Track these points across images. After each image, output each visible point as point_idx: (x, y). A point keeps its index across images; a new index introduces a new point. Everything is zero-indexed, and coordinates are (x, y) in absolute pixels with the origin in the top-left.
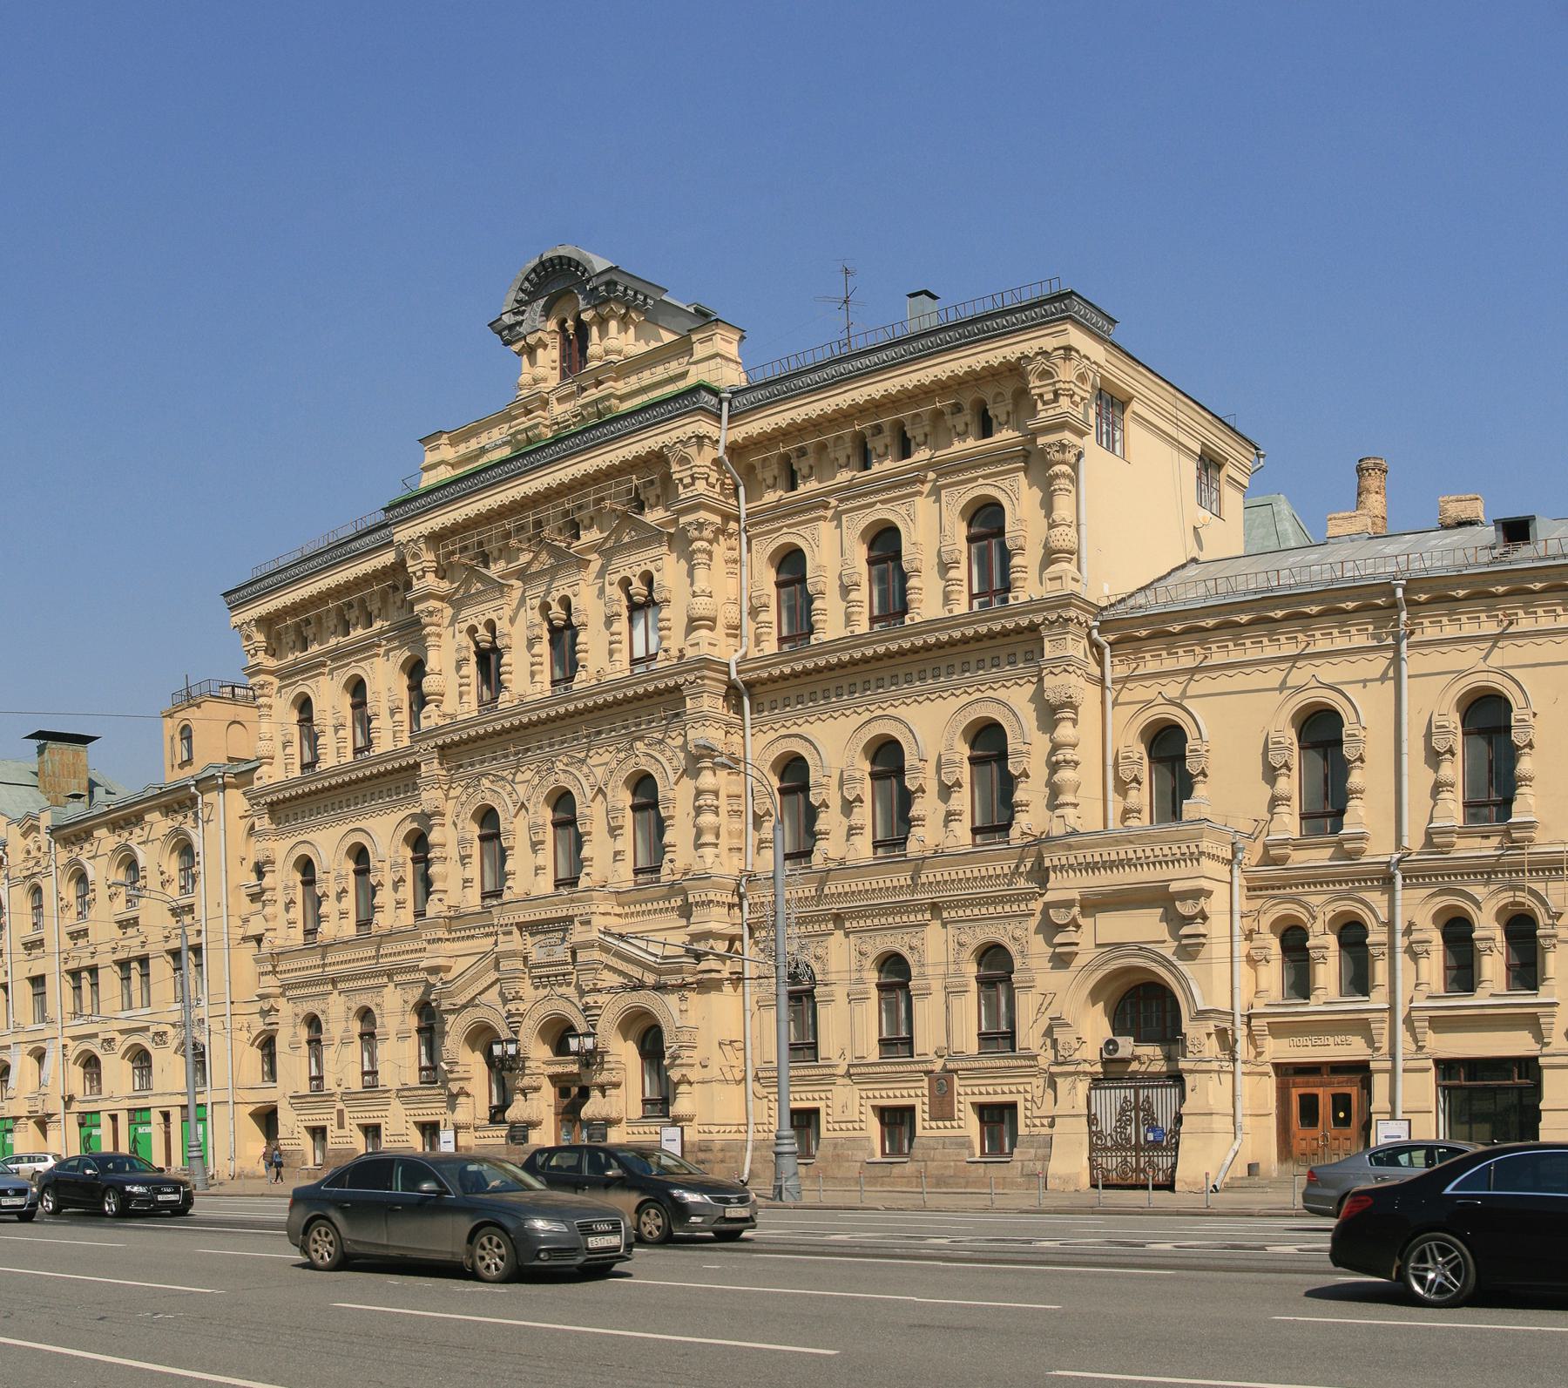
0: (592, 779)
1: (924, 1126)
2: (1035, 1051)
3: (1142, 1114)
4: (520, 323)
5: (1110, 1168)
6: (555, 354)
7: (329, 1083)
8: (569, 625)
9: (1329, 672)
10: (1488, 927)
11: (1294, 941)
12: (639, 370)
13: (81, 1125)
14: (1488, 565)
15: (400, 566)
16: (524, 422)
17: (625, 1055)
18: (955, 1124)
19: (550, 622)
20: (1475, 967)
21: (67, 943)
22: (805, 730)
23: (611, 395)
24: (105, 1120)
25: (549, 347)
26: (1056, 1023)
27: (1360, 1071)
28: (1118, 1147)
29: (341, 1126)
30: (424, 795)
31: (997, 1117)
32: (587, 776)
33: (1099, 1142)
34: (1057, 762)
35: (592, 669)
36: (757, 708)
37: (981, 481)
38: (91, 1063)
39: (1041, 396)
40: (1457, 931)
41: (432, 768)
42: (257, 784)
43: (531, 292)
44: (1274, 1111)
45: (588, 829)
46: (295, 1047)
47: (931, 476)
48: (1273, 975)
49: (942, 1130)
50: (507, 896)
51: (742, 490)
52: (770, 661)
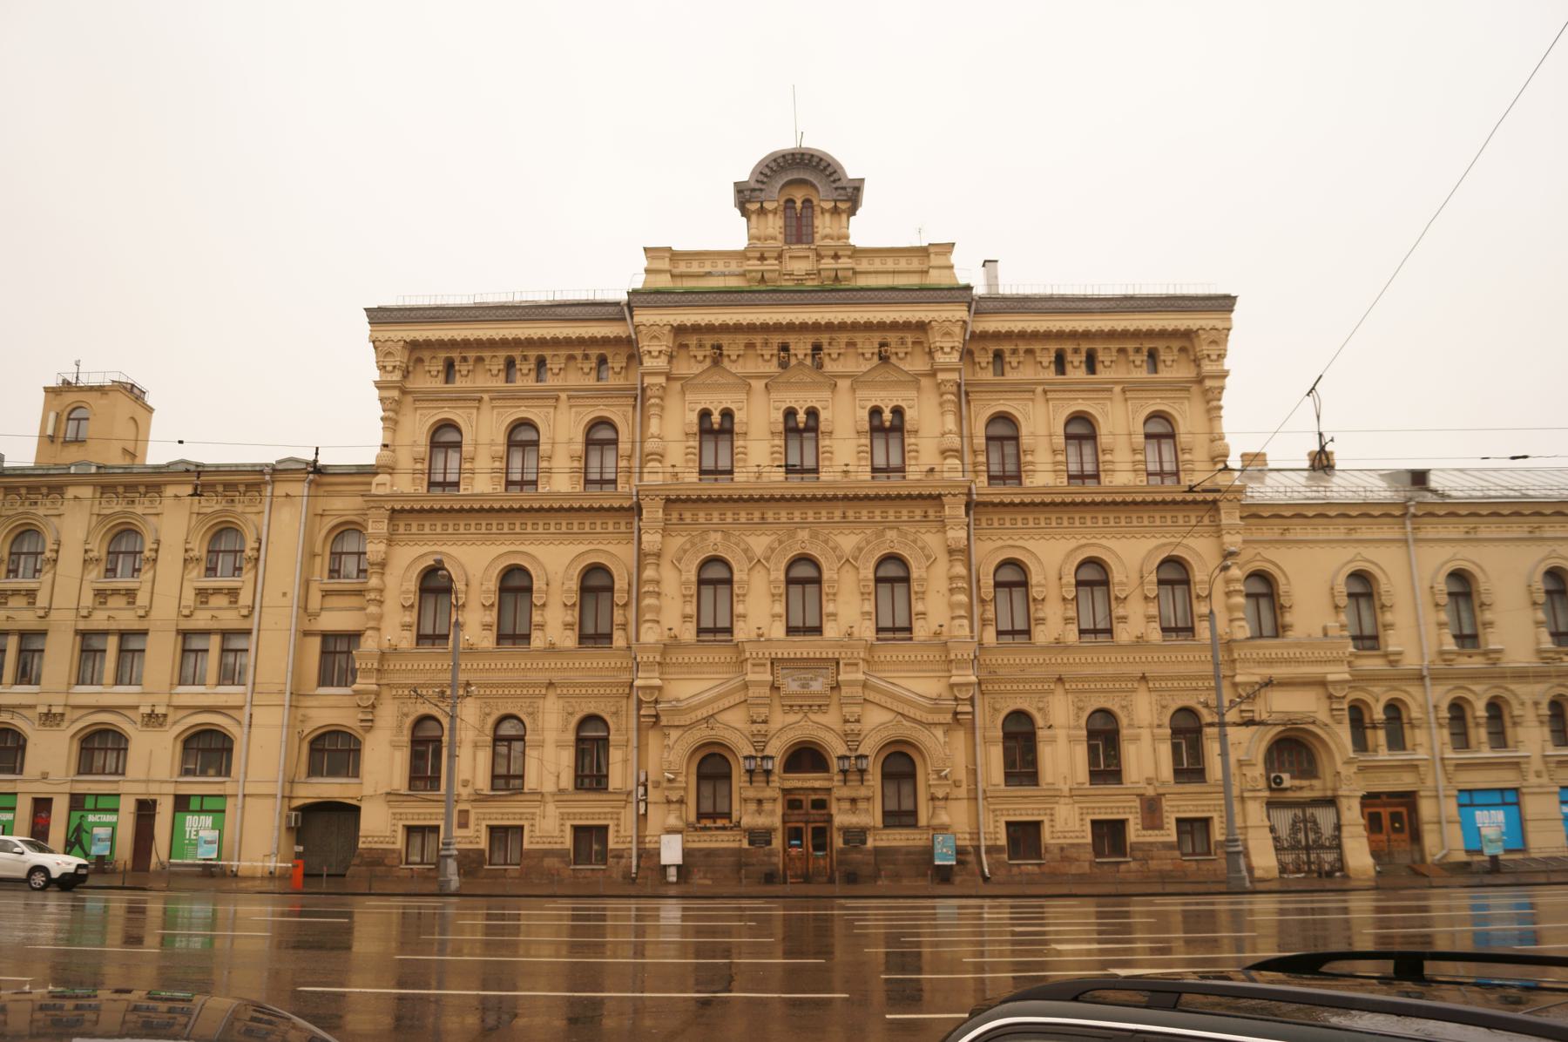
1: (1134, 833)
3: (1309, 825)
4: (761, 190)
9: (1371, 553)
16: (753, 265)
37: (1158, 401)
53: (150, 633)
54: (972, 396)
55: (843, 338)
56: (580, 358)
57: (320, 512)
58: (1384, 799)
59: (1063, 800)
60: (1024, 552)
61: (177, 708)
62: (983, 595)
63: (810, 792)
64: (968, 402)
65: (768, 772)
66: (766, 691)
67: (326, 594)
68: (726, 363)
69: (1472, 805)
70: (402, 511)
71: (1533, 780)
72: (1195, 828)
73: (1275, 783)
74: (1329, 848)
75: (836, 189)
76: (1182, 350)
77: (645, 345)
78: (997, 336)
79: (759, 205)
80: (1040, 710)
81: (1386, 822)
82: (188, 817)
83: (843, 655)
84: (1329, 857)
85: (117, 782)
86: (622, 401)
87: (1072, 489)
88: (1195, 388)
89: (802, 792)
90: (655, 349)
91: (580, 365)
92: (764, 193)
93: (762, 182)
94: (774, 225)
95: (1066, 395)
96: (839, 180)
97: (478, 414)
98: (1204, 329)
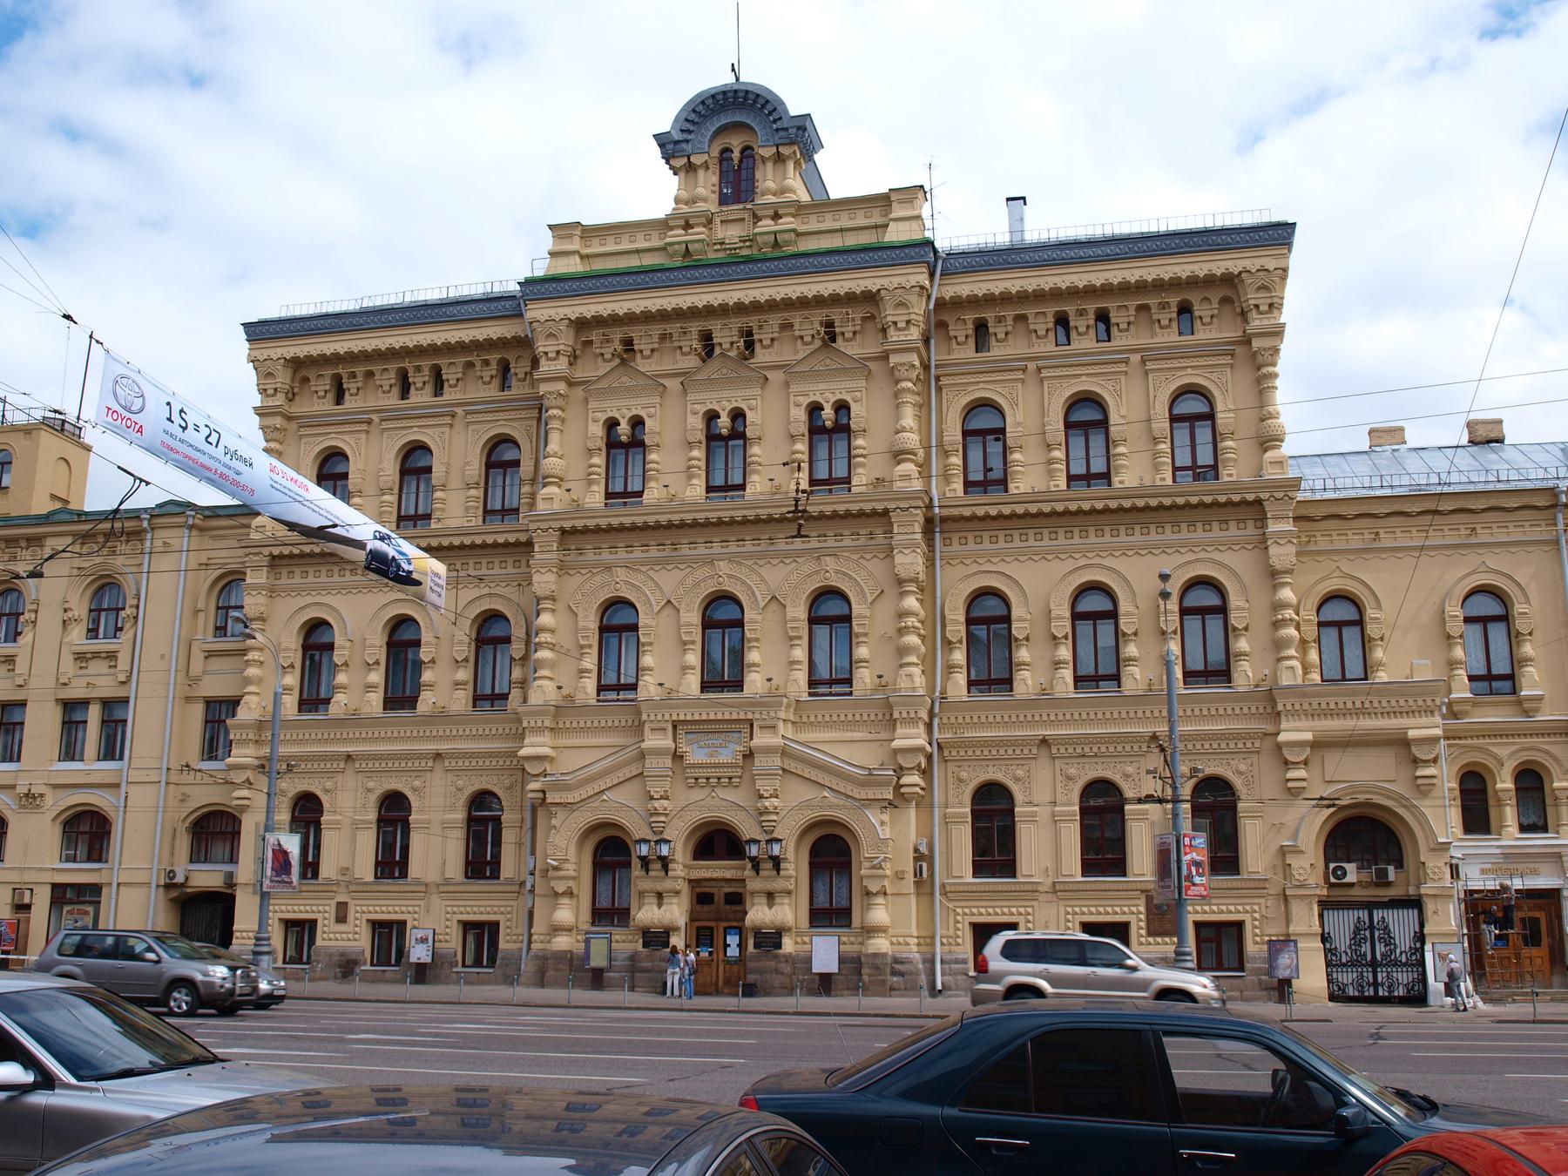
3: (1377, 934)
4: (687, 141)
5: (1345, 982)
6: (715, 179)
7: (327, 869)
16: (677, 236)
25: (710, 171)
28: (1353, 964)
29: (341, 918)
30: (536, 578)
33: (1334, 958)
36: (947, 542)
37: (502, 422)
43: (704, 116)
53: (28, 704)
54: (944, 381)
55: (775, 320)
56: (478, 365)
57: (205, 561)
59: (1042, 897)
60: (1002, 578)
61: (55, 786)
62: (1053, 630)
63: (723, 884)
64: (939, 389)
65: (665, 862)
66: (668, 762)
67: (210, 655)
68: (840, 344)
70: (281, 557)
75: (777, 130)
76: (1225, 301)
77: (541, 346)
78: (973, 302)
79: (685, 160)
80: (415, 790)
83: (757, 716)
84: (1404, 977)
85: (99, 870)
86: (523, 414)
87: (1071, 494)
88: (1239, 350)
89: (714, 884)
90: (551, 350)
91: (479, 374)
92: (690, 144)
93: (690, 132)
94: (707, 184)
95: (1066, 372)
96: (780, 118)
97: (367, 439)
98: (1249, 271)
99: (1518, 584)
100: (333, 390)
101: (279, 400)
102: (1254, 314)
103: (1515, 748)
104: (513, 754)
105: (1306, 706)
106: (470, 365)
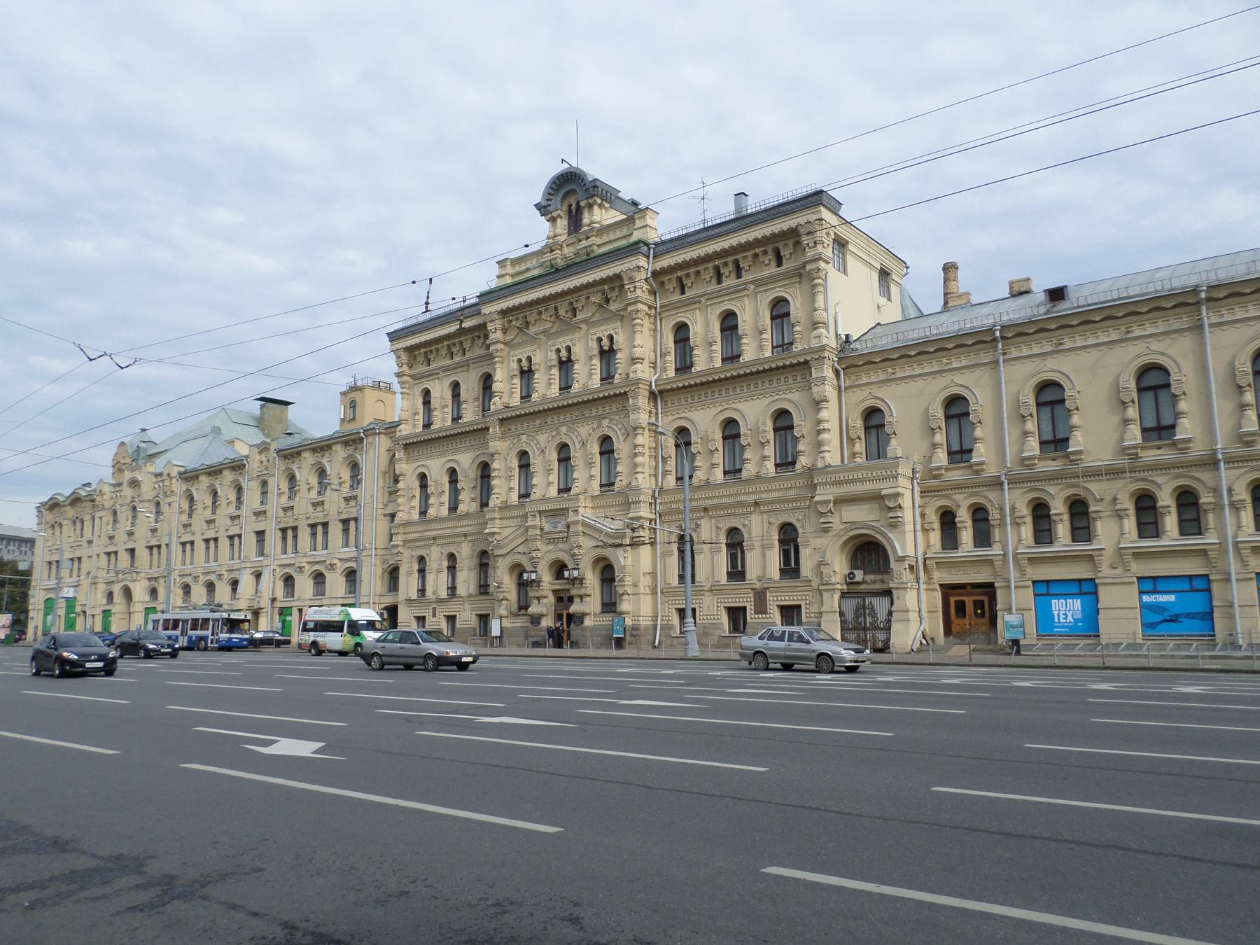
0: (579, 439)
1: (751, 616)
2: (811, 578)
3: (867, 611)
4: (549, 205)
6: (565, 222)
7: (429, 592)
8: (569, 360)
9: (960, 378)
10: (1058, 507)
11: (948, 520)
12: (607, 232)
13: (280, 614)
14: (1045, 314)
15: (483, 326)
16: (548, 256)
17: (592, 580)
18: (768, 616)
19: (560, 358)
20: (1053, 531)
21: (281, 513)
22: (688, 415)
23: (594, 244)
24: (295, 612)
26: (822, 563)
27: (988, 589)
28: (855, 628)
29: (434, 616)
30: (491, 444)
31: (790, 613)
32: (577, 437)
34: (820, 430)
35: (581, 382)
36: (664, 403)
37: (778, 289)
38: (289, 581)
39: (808, 244)
40: (1040, 511)
41: (495, 430)
42: (398, 434)
44: (940, 609)
45: (577, 463)
46: (409, 574)
47: (752, 287)
48: (935, 537)
49: (761, 619)
50: (532, 497)
51: (657, 294)
52: (671, 381)
58: (969, 589)
60: (687, 421)
64: (661, 320)
69: (1048, 594)
71: (1106, 571)
72: (790, 613)
73: (850, 578)
74: (882, 629)
81: (969, 608)
82: (1053, 601)
84: (881, 636)
94: (562, 224)
99: (1064, 374)
100: (775, 259)
101: (405, 368)
102: (807, 250)
103: (1025, 490)
104: (482, 533)
105: (828, 479)
106: (756, 256)
